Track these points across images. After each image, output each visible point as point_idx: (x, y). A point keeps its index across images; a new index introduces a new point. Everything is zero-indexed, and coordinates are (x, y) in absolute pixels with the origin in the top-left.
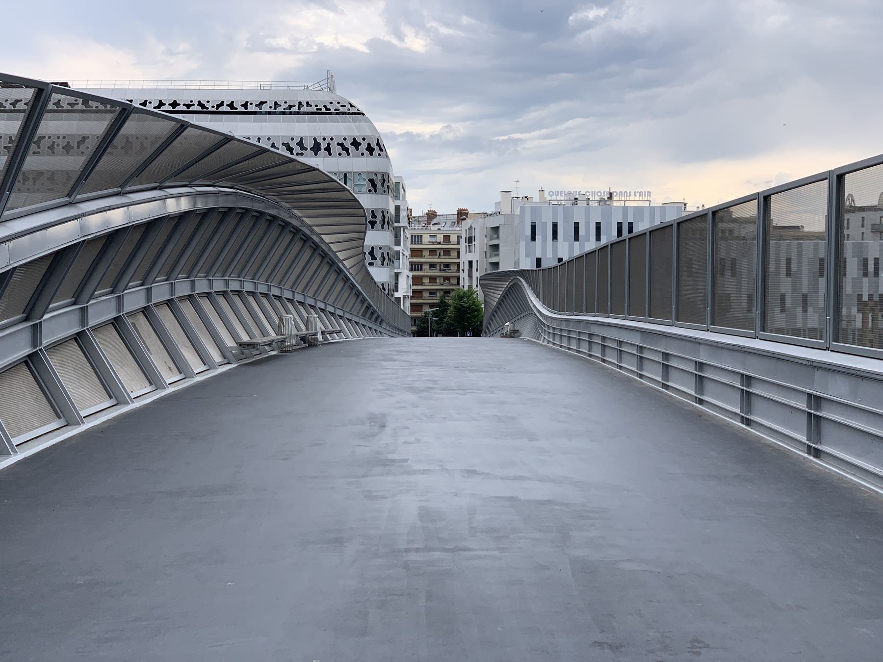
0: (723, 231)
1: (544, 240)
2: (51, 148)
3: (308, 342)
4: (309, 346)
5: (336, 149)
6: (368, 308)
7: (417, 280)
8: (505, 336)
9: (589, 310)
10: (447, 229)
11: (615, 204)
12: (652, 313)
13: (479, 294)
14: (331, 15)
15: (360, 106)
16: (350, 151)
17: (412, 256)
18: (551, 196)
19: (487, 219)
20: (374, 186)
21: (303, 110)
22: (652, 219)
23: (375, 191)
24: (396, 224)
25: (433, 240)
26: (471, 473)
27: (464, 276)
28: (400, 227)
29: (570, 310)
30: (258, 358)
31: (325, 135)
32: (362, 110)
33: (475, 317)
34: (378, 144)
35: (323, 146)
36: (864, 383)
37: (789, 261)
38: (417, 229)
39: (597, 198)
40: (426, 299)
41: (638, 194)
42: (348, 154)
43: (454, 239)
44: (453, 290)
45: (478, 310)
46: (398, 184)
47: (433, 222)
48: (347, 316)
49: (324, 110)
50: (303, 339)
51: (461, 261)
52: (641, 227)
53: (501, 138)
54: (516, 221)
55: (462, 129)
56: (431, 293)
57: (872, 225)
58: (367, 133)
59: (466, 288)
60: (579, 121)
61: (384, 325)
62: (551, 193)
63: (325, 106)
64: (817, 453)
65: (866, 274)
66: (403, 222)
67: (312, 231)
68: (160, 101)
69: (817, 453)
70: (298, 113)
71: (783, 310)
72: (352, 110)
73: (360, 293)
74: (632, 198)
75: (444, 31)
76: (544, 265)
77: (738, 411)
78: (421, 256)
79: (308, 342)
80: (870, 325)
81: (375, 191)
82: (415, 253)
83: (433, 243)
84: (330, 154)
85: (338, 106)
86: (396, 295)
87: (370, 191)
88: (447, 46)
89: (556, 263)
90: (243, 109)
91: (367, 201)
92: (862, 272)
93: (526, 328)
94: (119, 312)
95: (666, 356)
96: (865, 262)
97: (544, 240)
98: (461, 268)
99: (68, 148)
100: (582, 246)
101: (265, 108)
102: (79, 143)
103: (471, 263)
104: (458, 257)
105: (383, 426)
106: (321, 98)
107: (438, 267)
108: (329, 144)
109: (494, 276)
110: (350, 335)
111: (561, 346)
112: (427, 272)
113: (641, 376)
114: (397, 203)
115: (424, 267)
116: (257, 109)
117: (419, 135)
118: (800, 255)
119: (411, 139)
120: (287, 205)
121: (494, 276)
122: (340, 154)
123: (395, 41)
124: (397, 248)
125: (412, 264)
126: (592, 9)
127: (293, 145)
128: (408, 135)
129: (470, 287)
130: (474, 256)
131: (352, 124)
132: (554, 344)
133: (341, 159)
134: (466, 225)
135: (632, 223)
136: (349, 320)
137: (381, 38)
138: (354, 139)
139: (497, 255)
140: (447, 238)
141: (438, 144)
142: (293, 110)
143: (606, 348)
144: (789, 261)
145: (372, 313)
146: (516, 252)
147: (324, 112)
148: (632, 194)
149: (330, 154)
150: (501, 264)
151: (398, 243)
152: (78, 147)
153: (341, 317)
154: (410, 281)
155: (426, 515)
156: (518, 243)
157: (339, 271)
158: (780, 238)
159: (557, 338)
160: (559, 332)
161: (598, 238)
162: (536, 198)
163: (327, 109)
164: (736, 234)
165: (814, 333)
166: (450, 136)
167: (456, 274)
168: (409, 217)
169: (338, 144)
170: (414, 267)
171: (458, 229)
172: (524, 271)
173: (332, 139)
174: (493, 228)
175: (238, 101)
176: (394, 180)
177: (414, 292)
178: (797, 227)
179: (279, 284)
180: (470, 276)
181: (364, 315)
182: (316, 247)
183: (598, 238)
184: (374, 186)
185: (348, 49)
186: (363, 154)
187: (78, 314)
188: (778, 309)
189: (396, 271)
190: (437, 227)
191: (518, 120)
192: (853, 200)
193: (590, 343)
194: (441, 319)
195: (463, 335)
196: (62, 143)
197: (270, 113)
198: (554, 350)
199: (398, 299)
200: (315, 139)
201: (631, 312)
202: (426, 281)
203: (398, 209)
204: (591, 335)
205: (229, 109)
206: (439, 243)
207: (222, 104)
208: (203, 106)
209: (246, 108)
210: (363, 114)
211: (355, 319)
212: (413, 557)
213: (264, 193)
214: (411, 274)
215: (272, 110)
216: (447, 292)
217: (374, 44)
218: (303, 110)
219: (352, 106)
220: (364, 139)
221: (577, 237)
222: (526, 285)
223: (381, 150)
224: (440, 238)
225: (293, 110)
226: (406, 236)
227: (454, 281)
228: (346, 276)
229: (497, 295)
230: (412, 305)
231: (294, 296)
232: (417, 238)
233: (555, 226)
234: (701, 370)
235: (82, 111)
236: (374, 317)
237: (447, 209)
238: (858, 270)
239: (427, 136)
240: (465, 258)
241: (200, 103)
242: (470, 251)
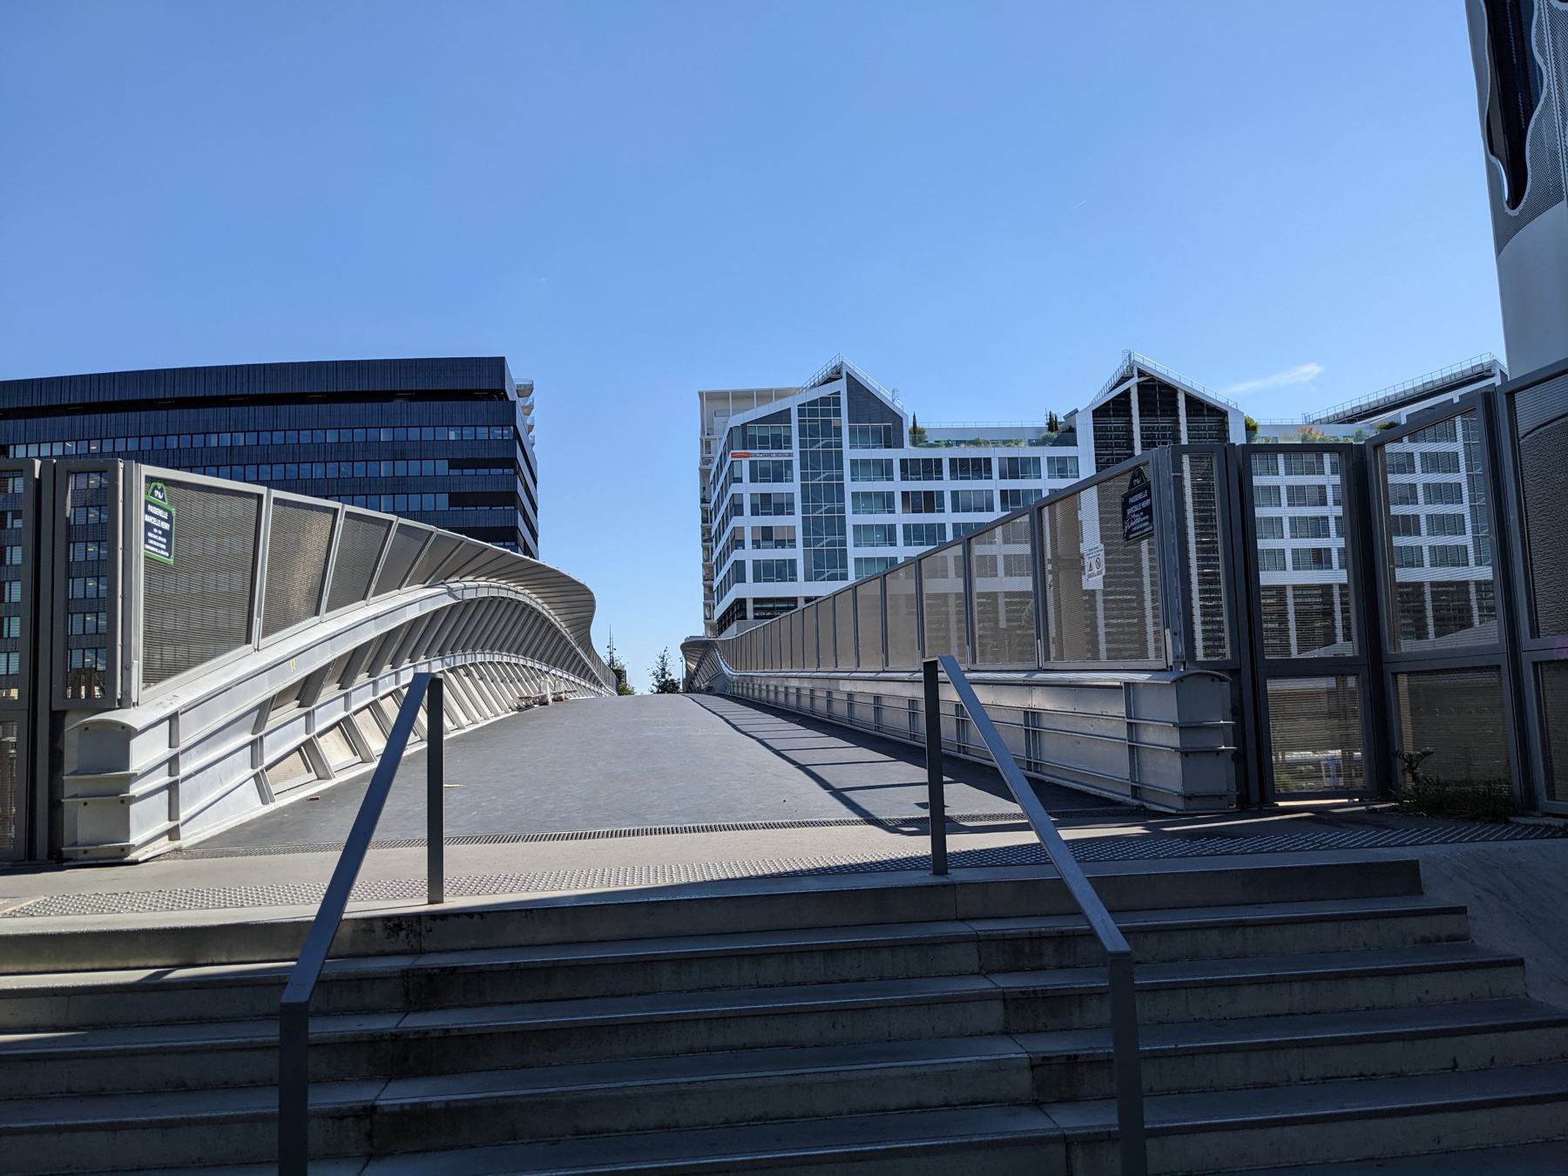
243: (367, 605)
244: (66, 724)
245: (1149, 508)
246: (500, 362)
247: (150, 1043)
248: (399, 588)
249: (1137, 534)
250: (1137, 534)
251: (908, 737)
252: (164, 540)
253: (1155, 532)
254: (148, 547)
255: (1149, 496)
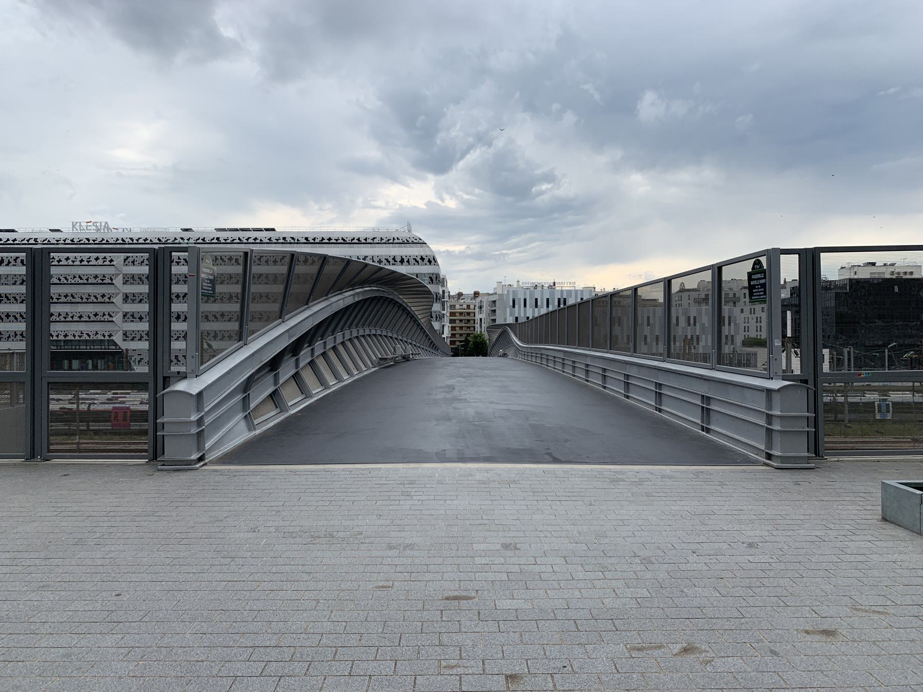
0: (615, 302)
1: (520, 307)
2: (267, 262)
3: (406, 359)
4: (407, 361)
5: (412, 261)
6: (431, 343)
7: (453, 328)
8: (498, 356)
9: (541, 342)
10: (468, 301)
11: (557, 288)
12: (568, 344)
13: (486, 337)
14: (406, 189)
15: (424, 239)
16: (419, 263)
17: (450, 316)
18: (523, 285)
19: (489, 296)
20: (432, 280)
21: (395, 242)
22: (576, 297)
23: (432, 283)
24: (443, 300)
25: (461, 307)
26: (492, 403)
27: (477, 326)
28: (444, 301)
29: (532, 343)
30: (386, 365)
31: (406, 254)
32: (426, 242)
33: (484, 347)
34: (434, 259)
35: (405, 261)
36: (643, 368)
37: (648, 318)
38: (453, 302)
39: (547, 286)
40: (458, 338)
41: (568, 284)
42: (419, 264)
43: (472, 307)
44: (472, 333)
45: (486, 344)
46: (443, 279)
47: (461, 298)
48: (422, 346)
49: (406, 242)
50: (404, 357)
51: (476, 318)
52: (571, 302)
53: (497, 253)
54: (505, 298)
55: (476, 248)
56: (460, 335)
57: (695, 299)
58: (429, 253)
59: (479, 333)
60: (538, 243)
61: (439, 351)
62: (523, 283)
63: (406, 240)
64: (628, 397)
65: (689, 325)
66: (446, 299)
67: (407, 305)
68: (323, 238)
69: (628, 397)
70: (392, 243)
71: (646, 344)
72: (420, 241)
73: (428, 335)
74: (566, 285)
75: (466, 197)
76: (519, 321)
77: (601, 383)
78: (455, 316)
79: (406, 359)
80: (687, 352)
81: (432, 283)
82: (452, 314)
83: (461, 309)
84: (409, 264)
85: (413, 240)
86: (443, 336)
87: (430, 283)
88: (467, 204)
89: (525, 320)
90: (365, 241)
91: (431, 288)
92: (687, 324)
93: (511, 352)
94: (335, 343)
95: (574, 362)
96: (689, 318)
97: (520, 307)
98: (476, 322)
99: (275, 262)
100: (539, 311)
101: (376, 241)
102: (281, 260)
103: (481, 319)
104: (474, 316)
105: (454, 389)
106: (404, 235)
107: (464, 321)
108: (409, 259)
109: (493, 326)
110: (424, 356)
111: (528, 360)
112: (458, 324)
113: (564, 372)
114: (443, 289)
115: (456, 322)
116: (372, 241)
117: (453, 252)
118: (654, 315)
119: (449, 253)
120: (396, 293)
121: (493, 326)
122: (414, 264)
123: (439, 202)
124: (443, 312)
125: (450, 320)
126: (544, 184)
127: (390, 259)
128: (447, 251)
129: (481, 332)
130: (483, 316)
131: (421, 249)
132: (524, 359)
133: (415, 267)
134: (478, 300)
135: (566, 299)
136: (423, 349)
137: (432, 201)
138: (422, 256)
139: (495, 315)
140: (468, 307)
141: (463, 256)
142: (390, 241)
143: (549, 360)
144: (648, 318)
145: (433, 345)
146: (505, 313)
147: (406, 243)
148: (566, 284)
149: (409, 264)
150: (497, 320)
151: (444, 310)
152: (281, 262)
153: (419, 347)
154: (450, 329)
155: (477, 413)
156: (506, 309)
157: (419, 325)
158: (644, 306)
159: (526, 356)
160: (527, 355)
161: (548, 306)
162: (515, 286)
163: (407, 241)
164: (622, 304)
165: (705, 358)
166: (469, 252)
167: (474, 325)
168: (449, 296)
169: (413, 259)
170: (452, 321)
171: (474, 301)
172: (509, 324)
173: (410, 256)
174: (493, 301)
175: (362, 238)
176: (442, 277)
177: (452, 334)
178: (655, 300)
179: (392, 331)
180: (481, 326)
181: (429, 346)
182: (409, 313)
183: (548, 306)
184: (432, 280)
185: (415, 207)
186: (426, 264)
187: (323, 344)
188: (643, 343)
189: (443, 324)
190: (463, 301)
191: (505, 243)
192: (684, 285)
193: (541, 358)
194: (466, 349)
195: (478, 356)
196: (272, 259)
197: (378, 243)
198: (526, 362)
199: (444, 338)
200: (401, 257)
201: (560, 343)
202: (457, 329)
203: (444, 291)
204: (542, 354)
205: (357, 242)
206: (464, 309)
207: (354, 239)
208: (344, 240)
209: (366, 241)
210: (426, 244)
211: (425, 348)
212: (475, 423)
213: (388, 289)
214: (450, 325)
215: (380, 242)
216: (468, 335)
217: (428, 204)
218: (395, 242)
219: (420, 239)
220: (426, 256)
221: (536, 306)
222: (510, 331)
223: (435, 262)
224: (465, 306)
225: (390, 241)
226: (447, 305)
227: (472, 329)
228: (422, 327)
229: (495, 336)
230: (451, 341)
231: (398, 336)
232: (453, 307)
233: (525, 300)
234: (587, 367)
235: (283, 243)
236: (434, 348)
237: (468, 291)
238: (685, 323)
239: (457, 253)
240: (478, 317)
241: (343, 239)
242: (481, 313)
243: (283, 322)
244: (205, 403)
245: (765, 284)
246: (748, 273)
247: (694, 428)
248: (307, 304)
249: (756, 297)
250: (756, 297)
251: (762, 369)
252: (211, 285)
253: (767, 299)
254: (203, 291)
255: (765, 278)
